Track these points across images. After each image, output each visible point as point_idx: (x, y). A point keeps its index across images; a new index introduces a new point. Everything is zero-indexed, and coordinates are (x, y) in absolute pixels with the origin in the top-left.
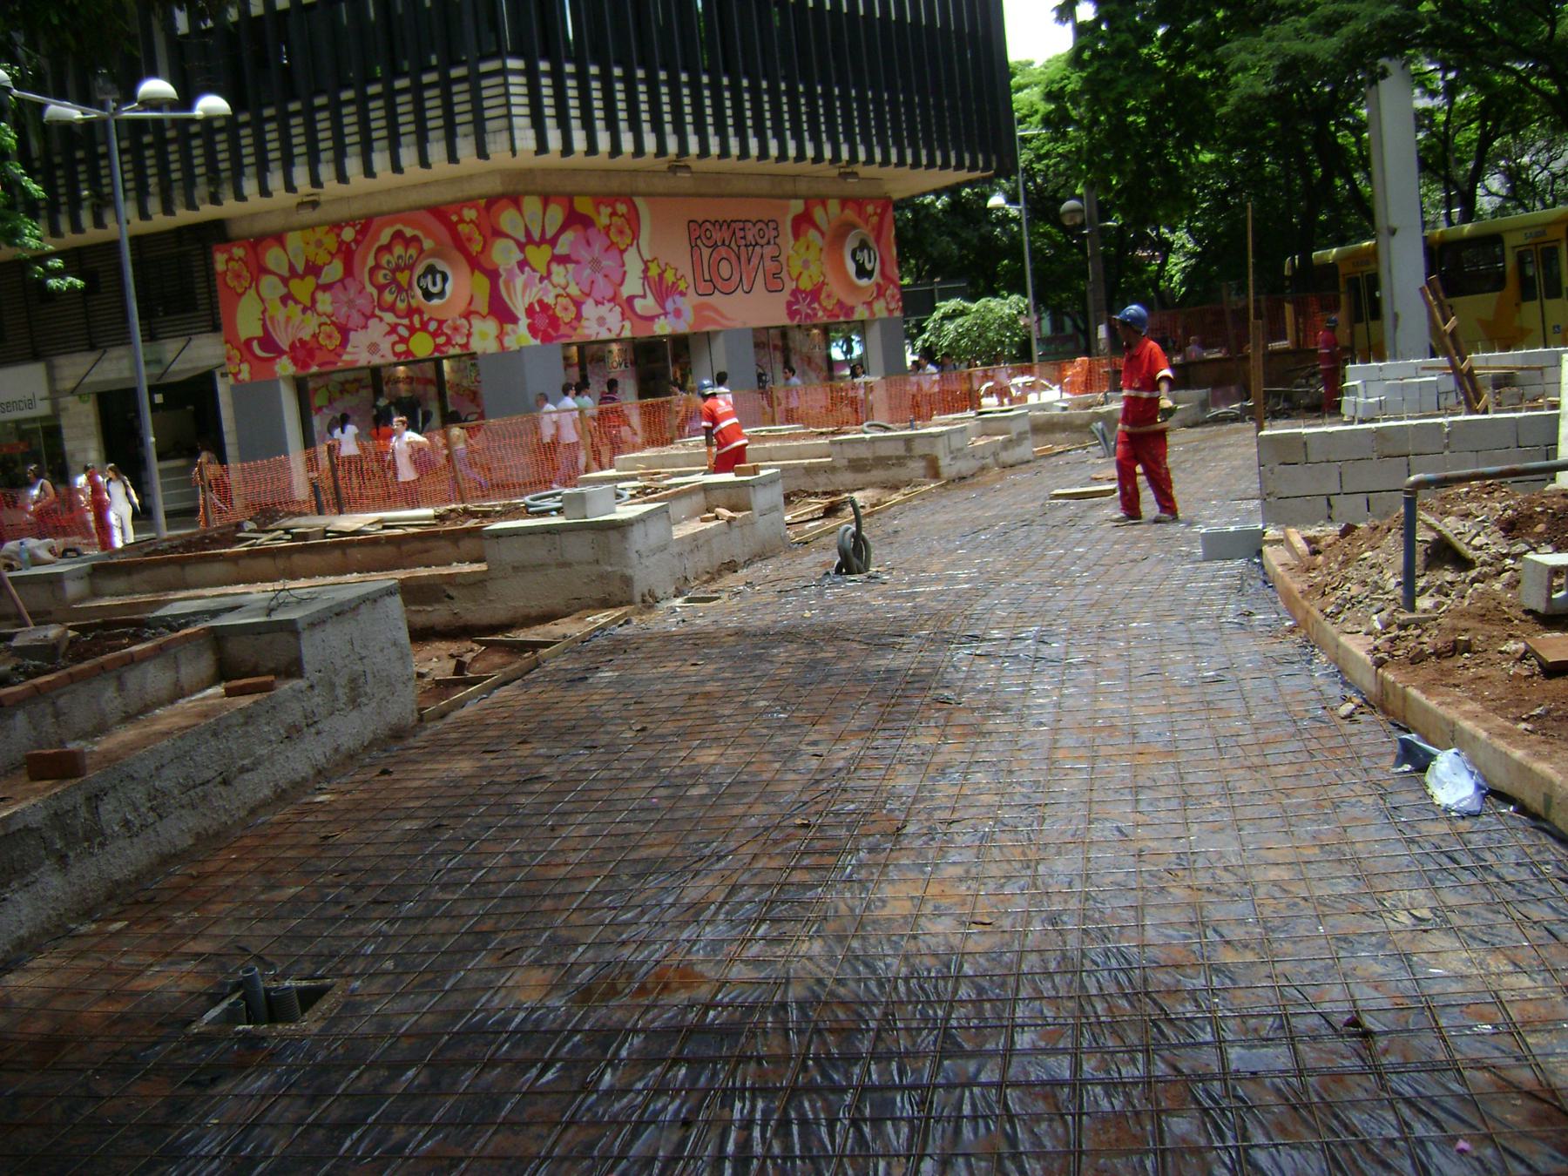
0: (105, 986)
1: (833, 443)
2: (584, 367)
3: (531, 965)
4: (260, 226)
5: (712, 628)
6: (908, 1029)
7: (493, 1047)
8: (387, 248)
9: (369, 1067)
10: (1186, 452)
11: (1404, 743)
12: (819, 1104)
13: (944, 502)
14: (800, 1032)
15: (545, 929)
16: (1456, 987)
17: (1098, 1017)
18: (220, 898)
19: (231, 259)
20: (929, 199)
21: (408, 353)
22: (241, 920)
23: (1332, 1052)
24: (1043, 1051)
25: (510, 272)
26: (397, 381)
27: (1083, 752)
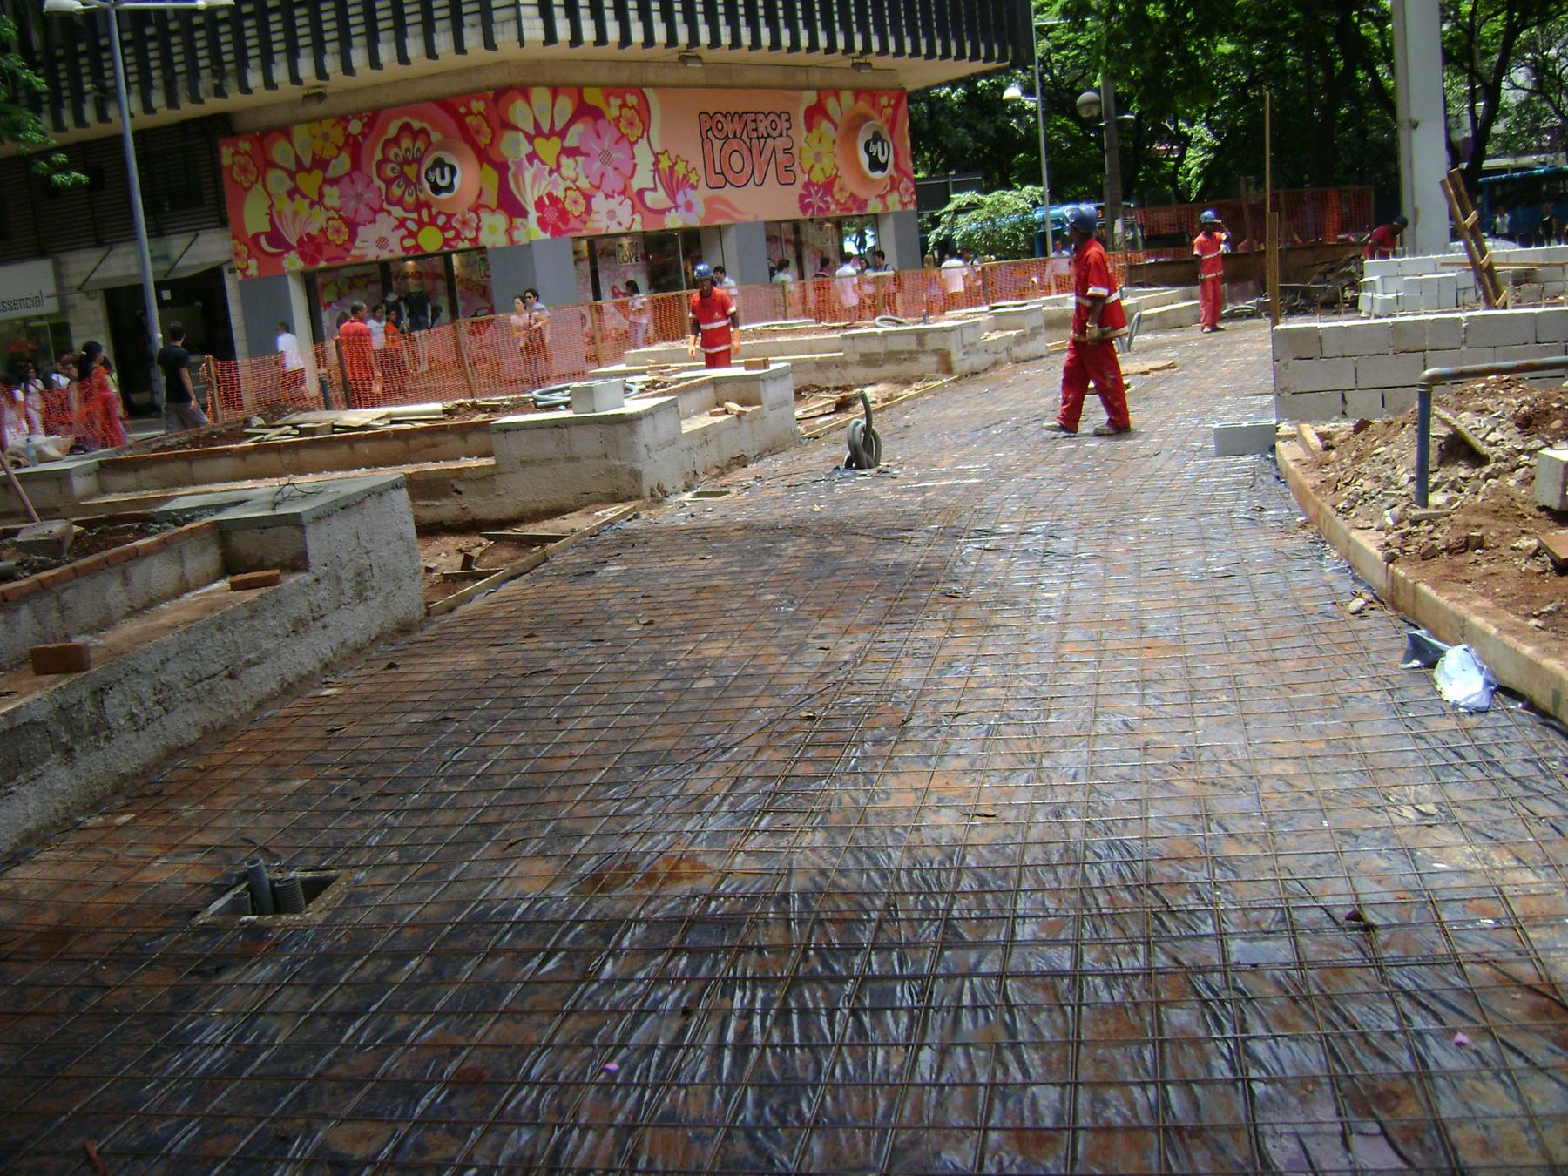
2: (598, 252)
5: (719, 523)
6: (909, 920)
7: (496, 937)
8: (395, 141)
9: (373, 957)
12: (819, 994)
13: (956, 396)
14: (801, 922)
15: (548, 821)
16: (1458, 882)
17: (1099, 909)
19: (237, 153)
21: (417, 247)
23: (1336, 946)
24: (1044, 942)
25: (519, 165)
26: (406, 276)
27: (1091, 646)
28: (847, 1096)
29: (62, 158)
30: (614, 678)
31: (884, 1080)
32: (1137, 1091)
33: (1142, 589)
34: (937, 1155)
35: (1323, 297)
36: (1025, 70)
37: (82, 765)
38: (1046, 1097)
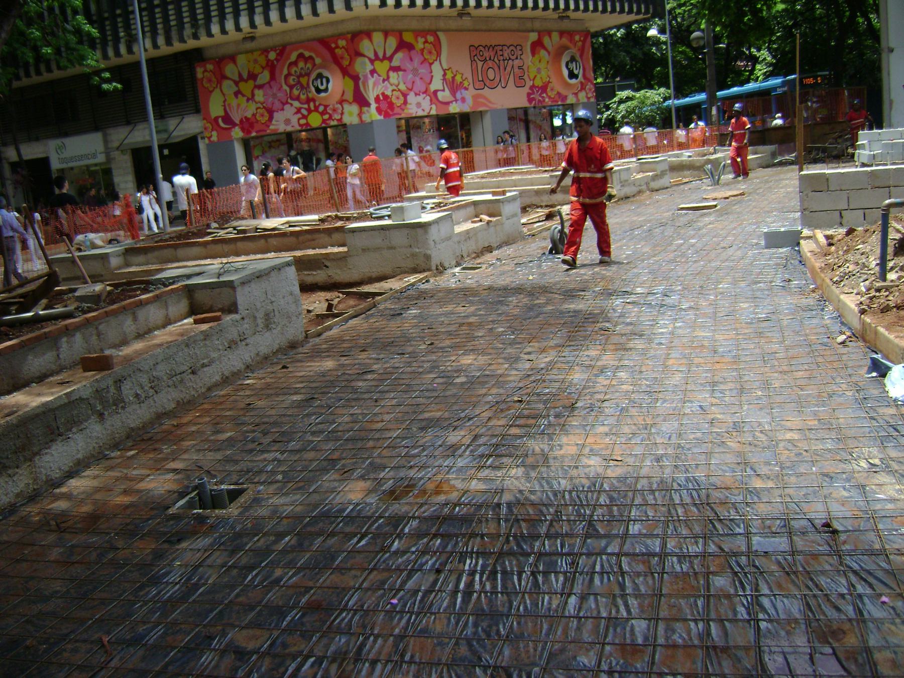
0: (123, 487)
1: (551, 176)
2: (410, 130)
3: (358, 479)
4: (222, 51)
5: (474, 285)
6: (569, 521)
7: (334, 525)
8: (295, 63)
9: (264, 535)
10: (760, 183)
11: (873, 359)
12: (514, 563)
13: (616, 211)
14: (506, 521)
15: (367, 458)
16: (890, 506)
17: (678, 517)
18: (189, 438)
19: (206, 71)
20: (612, 32)
21: (307, 124)
22: (199, 450)
23: (813, 542)
24: (645, 535)
25: (365, 77)
26: (301, 141)
27: (684, 361)
28: (526, 623)
29: (107, 75)
30: (408, 376)
31: (547, 614)
32: (692, 624)
33: (716, 328)
34: (575, 658)
35: (835, 153)
36: (660, 19)
37: (108, 423)
38: (639, 626)
